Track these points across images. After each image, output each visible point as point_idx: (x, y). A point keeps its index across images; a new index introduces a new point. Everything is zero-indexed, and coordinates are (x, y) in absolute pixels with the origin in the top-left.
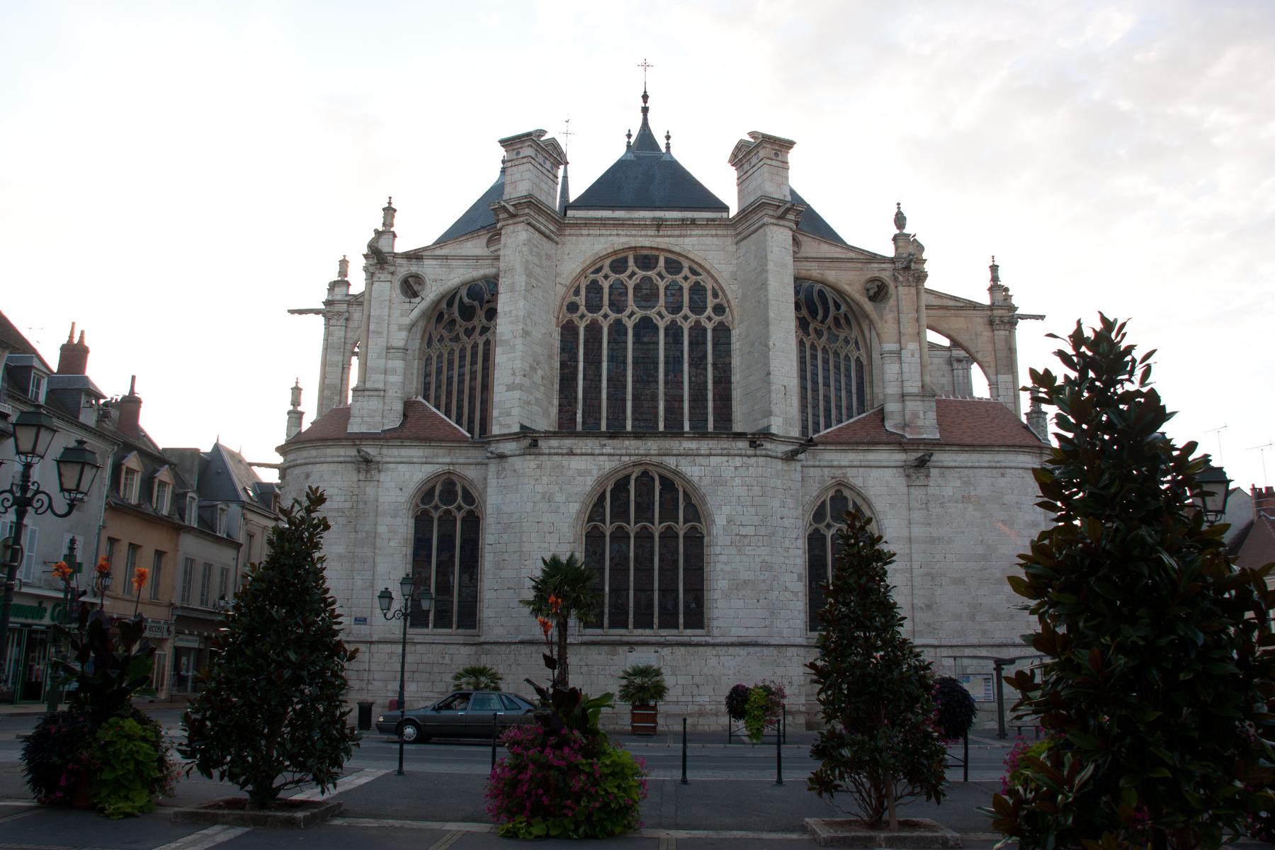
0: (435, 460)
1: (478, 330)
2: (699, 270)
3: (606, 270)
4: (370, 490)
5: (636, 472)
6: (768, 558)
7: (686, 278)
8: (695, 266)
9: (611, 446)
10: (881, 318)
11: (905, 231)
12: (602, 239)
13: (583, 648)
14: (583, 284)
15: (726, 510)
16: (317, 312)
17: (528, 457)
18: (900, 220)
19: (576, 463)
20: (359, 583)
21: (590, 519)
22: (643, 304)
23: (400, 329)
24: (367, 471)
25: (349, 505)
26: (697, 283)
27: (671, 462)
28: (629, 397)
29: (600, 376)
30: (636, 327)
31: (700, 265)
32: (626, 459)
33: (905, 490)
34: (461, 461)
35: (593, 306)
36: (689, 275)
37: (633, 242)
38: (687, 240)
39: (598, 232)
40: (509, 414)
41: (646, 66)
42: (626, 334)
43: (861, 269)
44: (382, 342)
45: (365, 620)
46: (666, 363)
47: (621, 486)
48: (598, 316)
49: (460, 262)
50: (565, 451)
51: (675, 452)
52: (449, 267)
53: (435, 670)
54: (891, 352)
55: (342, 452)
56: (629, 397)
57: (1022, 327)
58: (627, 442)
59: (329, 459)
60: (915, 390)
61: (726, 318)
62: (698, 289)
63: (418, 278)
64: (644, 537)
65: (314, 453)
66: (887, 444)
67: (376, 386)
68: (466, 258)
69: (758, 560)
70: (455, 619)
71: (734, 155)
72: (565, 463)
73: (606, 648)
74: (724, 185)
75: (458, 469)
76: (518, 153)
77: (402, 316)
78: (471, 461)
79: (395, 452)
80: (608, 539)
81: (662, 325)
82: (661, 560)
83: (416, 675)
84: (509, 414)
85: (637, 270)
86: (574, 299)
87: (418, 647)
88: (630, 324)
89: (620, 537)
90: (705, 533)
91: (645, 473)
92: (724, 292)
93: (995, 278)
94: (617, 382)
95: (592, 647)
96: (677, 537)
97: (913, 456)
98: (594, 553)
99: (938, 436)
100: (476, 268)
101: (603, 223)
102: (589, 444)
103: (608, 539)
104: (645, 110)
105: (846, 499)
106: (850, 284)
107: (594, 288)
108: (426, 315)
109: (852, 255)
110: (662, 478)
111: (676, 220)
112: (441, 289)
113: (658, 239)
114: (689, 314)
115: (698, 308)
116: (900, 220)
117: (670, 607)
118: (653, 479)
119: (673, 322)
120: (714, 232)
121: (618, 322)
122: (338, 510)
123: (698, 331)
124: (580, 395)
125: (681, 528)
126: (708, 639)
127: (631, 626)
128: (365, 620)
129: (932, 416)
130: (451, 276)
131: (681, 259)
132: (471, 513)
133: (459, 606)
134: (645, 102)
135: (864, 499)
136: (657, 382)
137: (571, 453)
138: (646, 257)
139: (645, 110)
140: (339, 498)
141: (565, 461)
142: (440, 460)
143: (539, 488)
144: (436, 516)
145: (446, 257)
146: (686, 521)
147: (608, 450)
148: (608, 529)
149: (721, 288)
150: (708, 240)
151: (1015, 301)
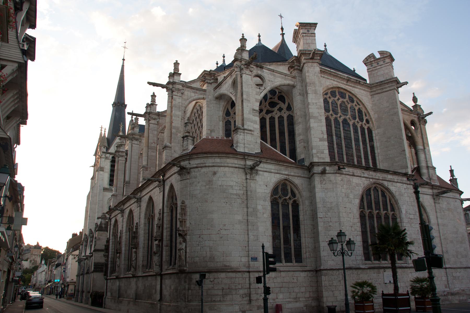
0: (281, 172)
2: (360, 103)
3: (329, 95)
8: (358, 101)
9: (366, 174)
10: (417, 135)
13: (368, 270)
15: (404, 206)
16: (162, 86)
17: (337, 175)
19: (355, 180)
21: (360, 208)
22: (343, 113)
23: (256, 101)
24: (251, 174)
25: (242, 192)
27: (386, 183)
31: (360, 101)
32: (371, 180)
33: (433, 204)
34: (292, 174)
36: (357, 104)
38: (356, 90)
39: (327, 77)
43: (409, 115)
49: (279, 75)
50: (351, 174)
51: (387, 179)
52: (274, 75)
53: (291, 286)
55: (236, 161)
59: (230, 165)
61: (371, 125)
62: (360, 111)
65: (218, 160)
67: (250, 128)
71: (366, 59)
72: (351, 179)
73: (376, 270)
74: (362, 71)
75: (291, 178)
77: (257, 94)
78: (296, 174)
80: (367, 218)
81: (351, 123)
83: (282, 289)
87: (282, 273)
92: (369, 114)
94: (339, 145)
95: (371, 270)
99: (439, 184)
100: (285, 79)
102: (358, 172)
104: (283, 34)
108: (265, 97)
109: (406, 109)
112: (272, 86)
113: (347, 86)
120: (364, 89)
122: (236, 194)
126: (405, 265)
128: (257, 258)
130: (276, 81)
131: (354, 97)
133: (295, 251)
134: (282, 31)
137: (353, 175)
139: (283, 34)
140: (236, 188)
141: (351, 178)
142: (283, 172)
143: (344, 191)
145: (273, 71)
147: (366, 175)
148: (367, 212)
149: (368, 112)
150: (362, 91)
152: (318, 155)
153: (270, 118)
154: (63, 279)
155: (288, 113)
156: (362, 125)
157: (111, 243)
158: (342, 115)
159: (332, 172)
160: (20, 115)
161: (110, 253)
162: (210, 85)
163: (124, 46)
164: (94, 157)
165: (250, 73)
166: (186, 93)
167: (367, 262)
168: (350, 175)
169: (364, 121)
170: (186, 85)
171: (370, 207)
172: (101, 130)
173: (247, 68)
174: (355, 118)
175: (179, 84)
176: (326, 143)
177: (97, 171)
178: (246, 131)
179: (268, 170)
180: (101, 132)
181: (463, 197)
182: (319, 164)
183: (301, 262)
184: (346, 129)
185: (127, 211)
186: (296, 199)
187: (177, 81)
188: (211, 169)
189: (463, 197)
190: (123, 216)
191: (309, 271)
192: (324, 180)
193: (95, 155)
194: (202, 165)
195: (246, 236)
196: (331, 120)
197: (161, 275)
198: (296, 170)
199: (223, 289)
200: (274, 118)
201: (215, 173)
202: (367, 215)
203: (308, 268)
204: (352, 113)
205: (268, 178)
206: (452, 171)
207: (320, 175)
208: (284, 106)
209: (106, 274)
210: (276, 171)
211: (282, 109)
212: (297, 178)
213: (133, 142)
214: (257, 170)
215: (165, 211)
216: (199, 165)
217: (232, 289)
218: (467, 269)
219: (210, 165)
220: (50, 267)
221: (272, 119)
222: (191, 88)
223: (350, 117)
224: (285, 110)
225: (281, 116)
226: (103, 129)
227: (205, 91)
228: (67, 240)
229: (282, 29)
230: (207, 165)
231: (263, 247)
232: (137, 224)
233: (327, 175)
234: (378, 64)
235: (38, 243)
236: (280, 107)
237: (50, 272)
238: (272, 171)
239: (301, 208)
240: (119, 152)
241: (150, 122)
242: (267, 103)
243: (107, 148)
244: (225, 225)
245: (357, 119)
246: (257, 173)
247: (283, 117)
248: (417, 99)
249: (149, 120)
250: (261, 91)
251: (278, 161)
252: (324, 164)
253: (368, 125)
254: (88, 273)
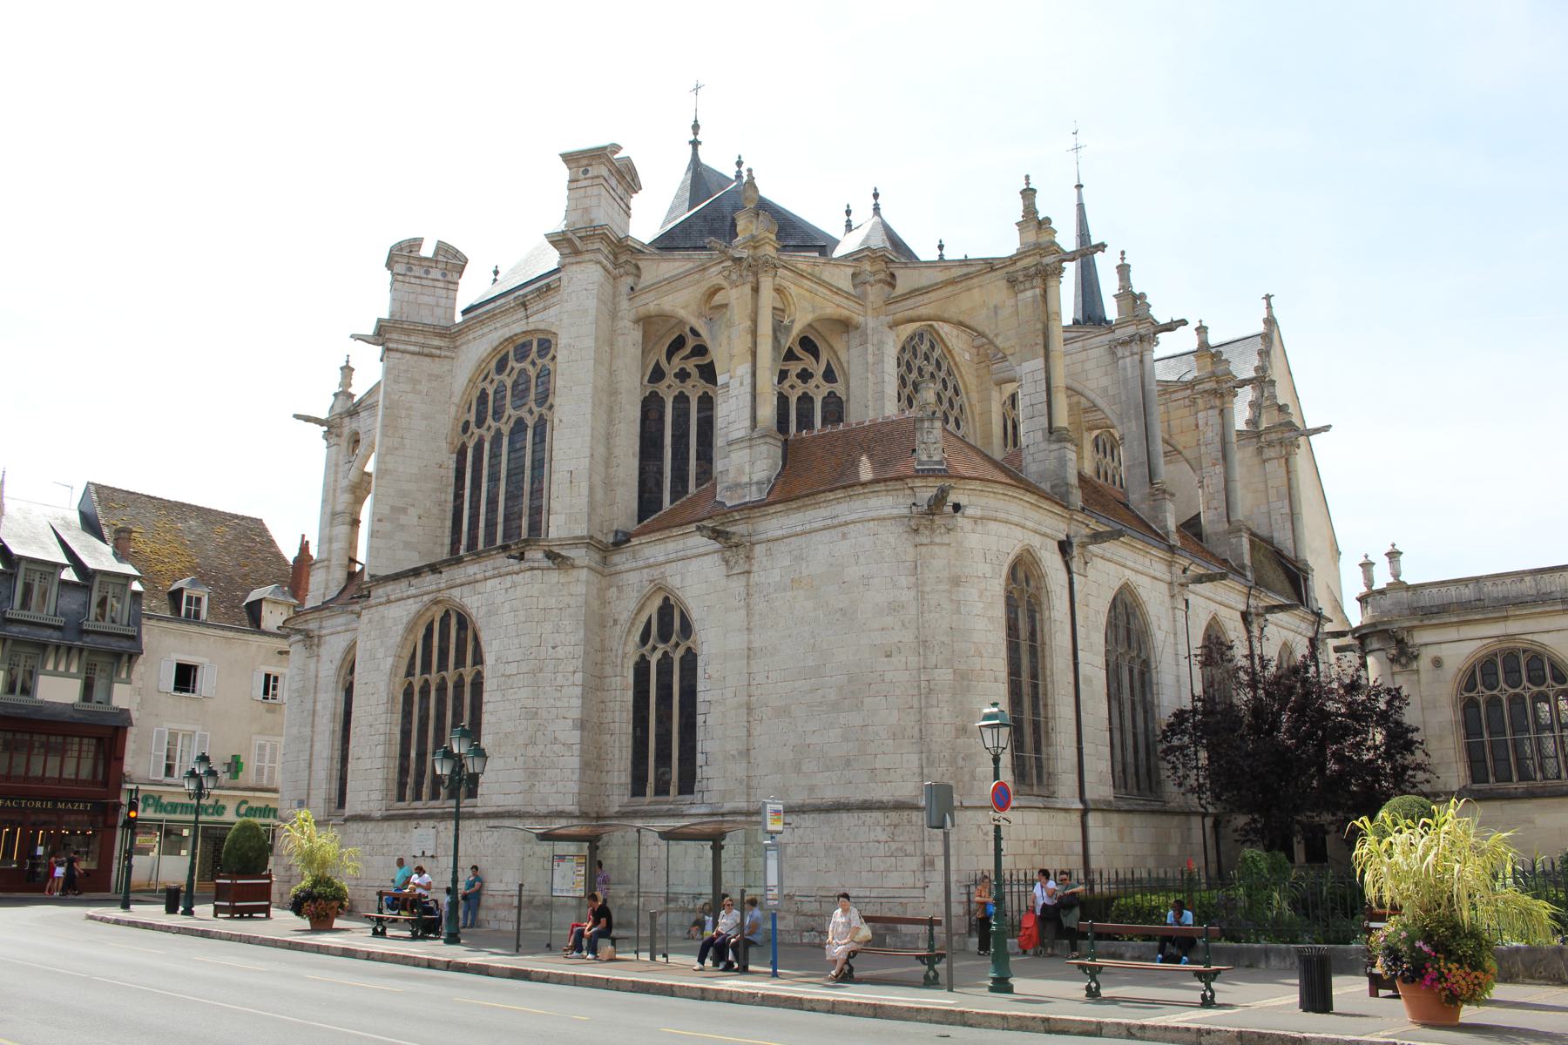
6: (529, 703)
12: (485, 339)
13: (386, 824)
32: (426, 598)
37: (507, 332)
38: (552, 311)
69: (519, 705)
73: (400, 824)
80: (1548, 675)
93: (1030, 210)
94: (493, 502)
95: (392, 823)
104: (695, 144)
134: (696, 134)
139: (695, 144)
147: (413, 591)
155: (826, 388)
195: (308, 729)
200: (687, 399)
208: (819, 370)
211: (811, 376)
218: (834, 816)
224: (818, 378)
225: (805, 394)
229: (696, 127)
234: (427, 272)
247: (811, 399)
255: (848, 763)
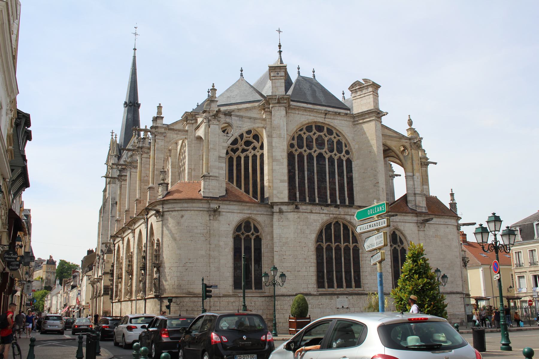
0: (244, 212)
1: (240, 150)
2: (339, 134)
3: (305, 130)
4: (215, 224)
5: (335, 221)
7: (335, 137)
8: (338, 133)
9: (326, 210)
11: (412, 127)
13: (320, 297)
14: (296, 136)
18: (410, 123)
19: (313, 217)
20: (213, 269)
21: (317, 241)
22: (319, 147)
23: (223, 148)
24: (214, 215)
25: (206, 231)
26: (339, 140)
28: (316, 187)
29: (304, 177)
30: (317, 157)
31: (340, 132)
32: (331, 216)
33: (417, 232)
34: (255, 212)
35: (300, 146)
36: (336, 136)
38: (336, 121)
40: (282, 193)
41: (279, 31)
42: (313, 160)
44: (216, 154)
45: (217, 286)
46: (329, 174)
47: (328, 227)
48: (302, 150)
50: (309, 211)
51: (350, 214)
54: (410, 176)
56: (316, 187)
57: (430, 166)
58: (332, 209)
60: (419, 192)
62: (339, 143)
63: (230, 125)
64: (338, 249)
66: (235, 201)
67: (215, 175)
68: (250, 118)
70: (253, 285)
72: (309, 216)
73: (329, 297)
75: (253, 216)
76: (278, 74)
77: (224, 142)
79: (225, 207)
80: (325, 250)
81: (327, 157)
82: (345, 259)
84: (282, 193)
85: (316, 132)
86: (292, 142)
88: (315, 155)
89: (329, 249)
90: (360, 248)
91: (337, 222)
95: (324, 297)
96: (332, 249)
97: (421, 219)
98: (320, 256)
101: (305, 109)
102: (317, 209)
103: (325, 250)
105: (396, 235)
106: (395, 147)
107: (300, 138)
109: (395, 135)
110: (344, 225)
111: (333, 112)
114: (337, 153)
115: (340, 151)
116: (410, 123)
117: (348, 279)
118: (340, 225)
119: (331, 156)
121: (310, 154)
122: (200, 234)
123: (340, 161)
124: (297, 185)
125: (351, 246)
127: (345, 287)
128: (217, 286)
129: (425, 202)
130: (244, 126)
131: (333, 129)
132: (257, 236)
134: (280, 48)
135: (404, 235)
136: (326, 182)
137: (311, 212)
138: (319, 126)
139: (280, 52)
141: (309, 215)
142: (246, 212)
144: (243, 237)
146: (353, 243)
148: (324, 245)
149: (349, 143)
150: (343, 122)
151: (427, 156)
152: (278, 195)
153: (245, 157)
154: (79, 302)
156: (340, 157)
157: (115, 268)
158: (317, 149)
159: (289, 211)
160: (26, 161)
161: (115, 278)
162: (191, 125)
163: (134, 32)
164: (106, 166)
165: (218, 123)
166: (168, 135)
167: (320, 289)
168: (308, 213)
169: (344, 152)
170: (169, 128)
171: (329, 239)
172: (112, 135)
173: (215, 118)
174: (331, 151)
175: (161, 127)
176: (286, 184)
177: (109, 183)
178: (211, 178)
179: (231, 211)
180: (112, 138)
181: (460, 222)
182: (277, 204)
183: (261, 289)
184: (321, 163)
185: (137, 232)
186: (258, 234)
187: (159, 125)
188: (179, 212)
189: (460, 222)
190: (123, 243)
191: (268, 297)
192: (282, 218)
193: (107, 163)
194: (172, 209)
196: (303, 156)
197: (145, 300)
198: (259, 209)
199: (187, 310)
200: (248, 157)
201: (182, 216)
202: (324, 247)
203: (266, 294)
204: (330, 146)
205: (232, 216)
206: (452, 195)
207: (278, 214)
209: (111, 298)
210: (239, 211)
211: (256, 148)
212: (259, 216)
213: (132, 170)
214: (220, 212)
215: (148, 245)
216: (170, 209)
217: (194, 310)
218: (450, 295)
219: (179, 209)
220: (65, 289)
221: (247, 158)
222: (173, 130)
223: (327, 151)
225: (254, 154)
226: (114, 134)
227: (187, 131)
228: (82, 258)
229: (280, 46)
230: (176, 209)
231: (203, 280)
232: (158, 240)
233: (284, 214)
235: (51, 257)
236: (254, 146)
237: (65, 295)
238: (235, 211)
239: (263, 242)
240: (122, 176)
241: (143, 156)
242: (243, 142)
243: (118, 156)
244: (190, 259)
245: (335, 151)
246: (219, 215)
248: (412, 122)
249: (142, 155)
250: (228, 138)
251: (240, 201)
252: (283, 203)
253: (347, 156)
254: (99, 296)
255: (452, 282)
